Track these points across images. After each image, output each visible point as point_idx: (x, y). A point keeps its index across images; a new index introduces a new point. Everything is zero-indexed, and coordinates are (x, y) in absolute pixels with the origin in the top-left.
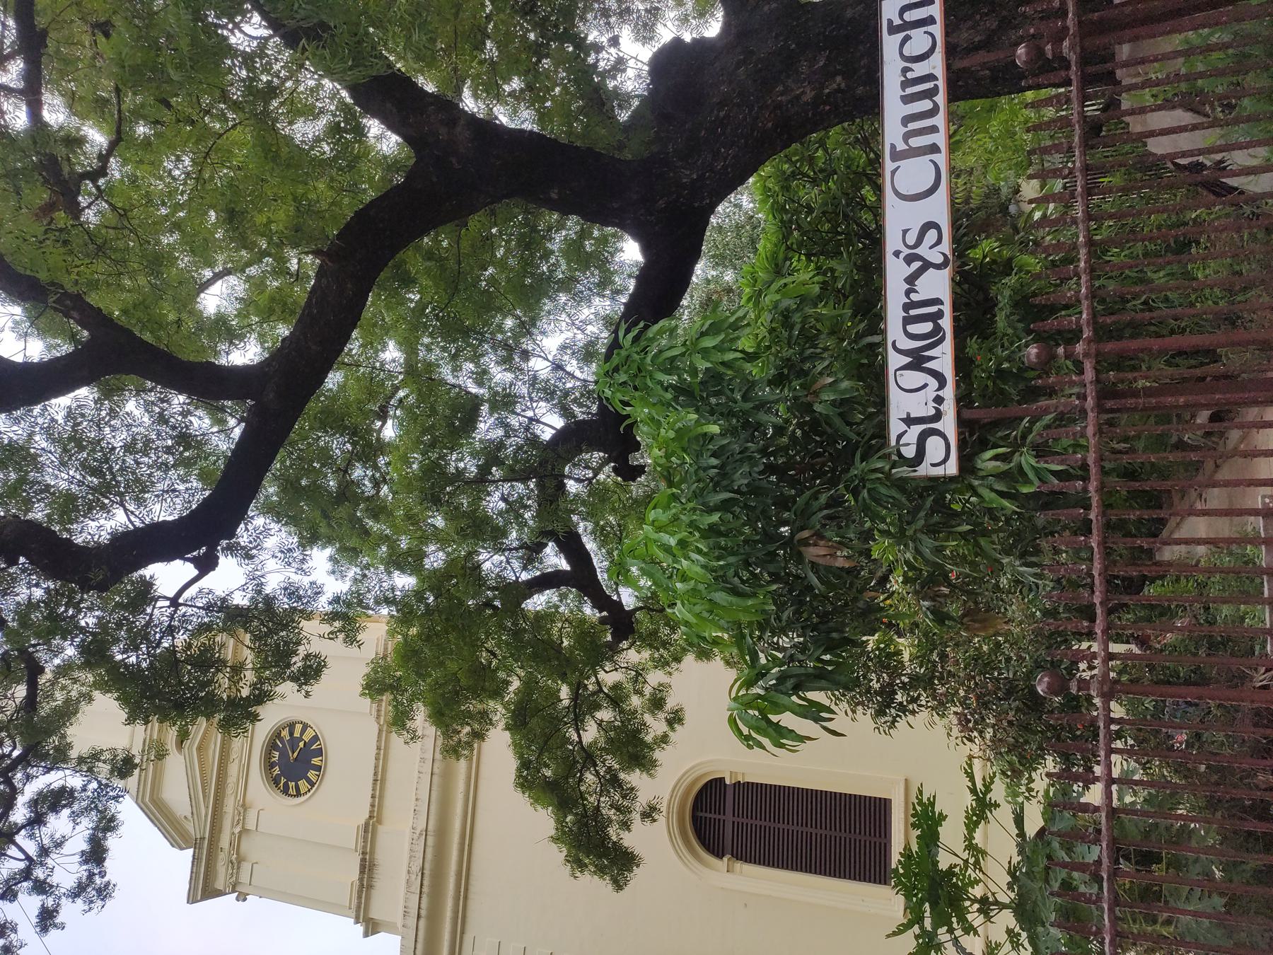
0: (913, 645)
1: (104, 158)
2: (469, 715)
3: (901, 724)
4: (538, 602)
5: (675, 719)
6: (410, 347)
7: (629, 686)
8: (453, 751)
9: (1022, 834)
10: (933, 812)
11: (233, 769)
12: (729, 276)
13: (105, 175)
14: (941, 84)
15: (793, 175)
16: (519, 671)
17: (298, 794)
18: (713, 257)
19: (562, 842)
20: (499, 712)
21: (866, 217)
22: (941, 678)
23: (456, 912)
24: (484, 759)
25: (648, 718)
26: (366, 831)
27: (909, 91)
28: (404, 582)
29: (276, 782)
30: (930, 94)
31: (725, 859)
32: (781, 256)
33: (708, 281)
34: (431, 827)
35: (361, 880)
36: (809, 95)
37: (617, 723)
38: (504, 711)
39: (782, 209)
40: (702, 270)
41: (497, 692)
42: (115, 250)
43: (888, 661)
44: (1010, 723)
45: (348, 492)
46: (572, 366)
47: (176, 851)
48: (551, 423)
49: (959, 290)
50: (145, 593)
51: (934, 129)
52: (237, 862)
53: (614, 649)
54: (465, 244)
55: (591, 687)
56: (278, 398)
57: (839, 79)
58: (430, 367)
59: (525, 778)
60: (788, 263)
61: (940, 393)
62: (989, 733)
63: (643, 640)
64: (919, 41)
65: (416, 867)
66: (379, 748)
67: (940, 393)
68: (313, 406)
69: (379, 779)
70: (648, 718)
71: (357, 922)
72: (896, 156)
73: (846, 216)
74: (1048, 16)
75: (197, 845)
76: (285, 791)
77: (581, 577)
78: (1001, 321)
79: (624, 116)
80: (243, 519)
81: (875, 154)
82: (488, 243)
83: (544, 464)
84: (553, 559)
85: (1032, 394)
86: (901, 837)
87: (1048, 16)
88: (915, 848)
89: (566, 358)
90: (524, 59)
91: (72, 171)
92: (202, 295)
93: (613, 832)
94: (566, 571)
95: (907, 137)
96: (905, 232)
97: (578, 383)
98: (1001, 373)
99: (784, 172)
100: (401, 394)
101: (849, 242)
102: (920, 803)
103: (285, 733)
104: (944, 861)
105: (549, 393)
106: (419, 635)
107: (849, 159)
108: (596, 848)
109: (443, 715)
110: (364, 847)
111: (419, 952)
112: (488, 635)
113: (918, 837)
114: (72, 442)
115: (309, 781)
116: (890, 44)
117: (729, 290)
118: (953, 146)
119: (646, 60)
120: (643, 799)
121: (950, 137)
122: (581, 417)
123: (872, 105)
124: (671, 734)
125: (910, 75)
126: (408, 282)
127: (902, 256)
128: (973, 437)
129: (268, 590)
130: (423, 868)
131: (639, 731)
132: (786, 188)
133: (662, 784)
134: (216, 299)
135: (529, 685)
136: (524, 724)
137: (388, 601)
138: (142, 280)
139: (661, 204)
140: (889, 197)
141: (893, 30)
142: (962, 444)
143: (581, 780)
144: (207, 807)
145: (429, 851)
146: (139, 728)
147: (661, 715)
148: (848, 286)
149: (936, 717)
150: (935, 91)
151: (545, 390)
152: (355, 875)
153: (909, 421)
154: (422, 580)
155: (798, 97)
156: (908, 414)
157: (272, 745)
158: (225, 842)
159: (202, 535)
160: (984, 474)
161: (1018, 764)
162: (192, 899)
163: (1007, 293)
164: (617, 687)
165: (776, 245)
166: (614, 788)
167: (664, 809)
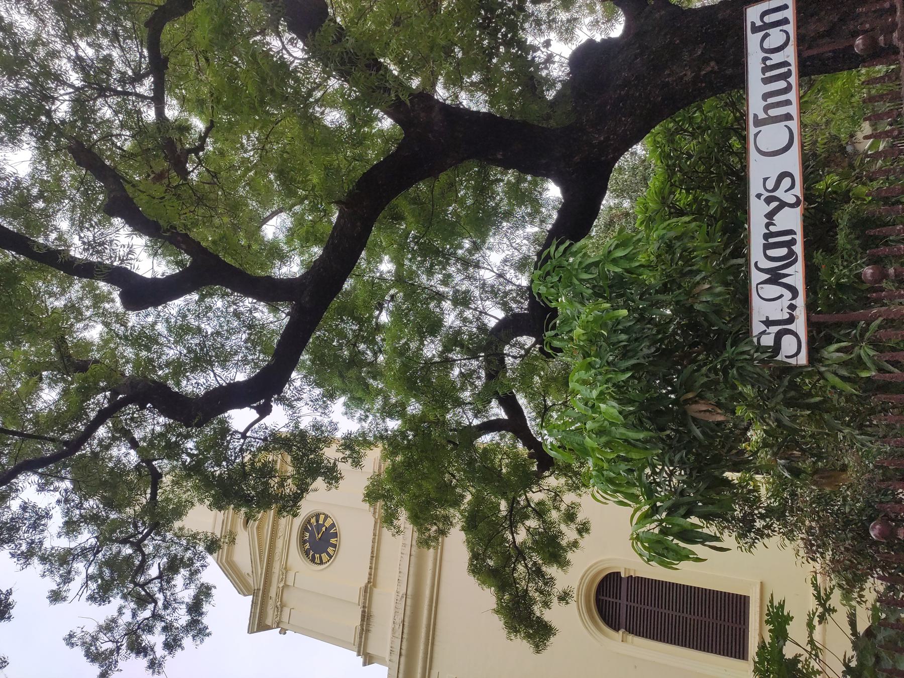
0: (769, 483)
1: (203, 139)
2: (437, 517)
3: (759, 544)
4: (486, 439)
5: (583, 529)
6: (398, 261)
7: (549, 503)
8: (425, 543)
9: (854, 633)
10: (783, 612)
11: (280, 543)
12: (626, 204)
13: (203, 149)
14: (793, 68)
15: (677, 131)
16: (471, 489)
17: (321, 563)
18: (614, 190)
19: (502, 614)
20: (457, 517)
21: (733, 160)
22: (791, 511)
23: (426, 653)
24: (445, 548)
25: (563, 527)
26: (366, 592)
27: (768, 74)
28: (393, 424)
29: (307, 553)
30: (785, 76)
31: (621, 632)
32: (666, 191)
33: (611, 208)
35: (362, 625)
36: (690, 75)
37: (540, 530)
38: (460, 517)
39: (668, 157)
40: (608, 201)
41: (456, 502)
42: (210, 200)
43: (751, 499)
44: (847, 549)
45: (356, 361)
46: (511, 274)
47: (241, 596)
48: (495, 315)
49: (807, 214)
50: (224, 430)
51: (788, 103)
52: (280, 608)
53: (539, 476)
54: (437, 191)
55: (522, 503)
56: (312, 299)
57: (713, 63)
58: (412, 273)
59: (475, 566)
60: (672, 196)
61: (793, 302)
62: (829, 555)
63: (561, 470)
64: (776, 37)
65: (399, 620)
66: (375, 535)
67: (793, 302)
68: (335, 303)
69: (375, 557)
70: (563, 527)
71: (359, 655)
72: (758, 123)
73: (717, 161)
74: (882, 13)
75: (255, 594)
76: (313, 560)
77: (515, 424)
78: (841, 239)
79: (550, 95)
80: (288, 381)
81: (740, 113)
82: (452, 187)
83: (490, 344)
84: (497, 411)
85: (866, 303)
86: (756, 632)
87: (882, 13)
88: (768, 640)
89: (506, 268)
90: (481, 60)
91: (182, 149)
92: (264, 227)
93: (537, 609)
94: (504, 420)
95: (766, 108)
96: (765, 180)
97: (514, 287)
98: (840, 286)
99: (669, 130)
100: (392, 292)
101: (720, 180)
102: (772, 606)
103: (313, 521)
104: (789, 651)
105: (492, 292)
106: (402, 463)
107: (719, 118)
108: (524, 619)
109: (419, 518)
110: (364, 603)
111: (401, 676)
112: (450, 462)
113: (770, 631)
114: (181, 331)
115: (328, 554)
116: (753, 41)
117: (627, 214)
118: (803, 107)
119: (567, 56)
120: (559, 587)
121: (801, 98)
122: (517, 311)
123: (739, 80)
124: (580, 541)
125: (768, 63)
126: (398, 217)
127: (763, 198)
128: (819, 336)
129: (302, 426)
130: (404, 621)
131: (556, 537)
132: (671, 141)
133: (574, 575)
134: (274, 229)
135: (478, 500)
136: (475, 527)
137: (382, 437)
138: (226, 219)
139: (577, 159)
140: (753, 154)
141: (755, 29)
142: (811, 340)
143: (514, 569)
144: (262, 568)
145: (408, 608)
146: (220, 515)
147: (573, 526)
148: (719, 212)
149: (787, 542)
150: (788, 74)
151: (492, 292)
152: (358, 622)
153: (768, 323)
154: (405, 422)
155: (681, 78)
156: (767, 317)
157: (304, 529)
158: (273, 593)
159: (263, 390)
160: (830, 362)
161: (852, 582)
162: (251, 631)
163: (846, 217)
164: (541, 503)
165: (663, 183)
166: (538, 577)
167: (575, 595)
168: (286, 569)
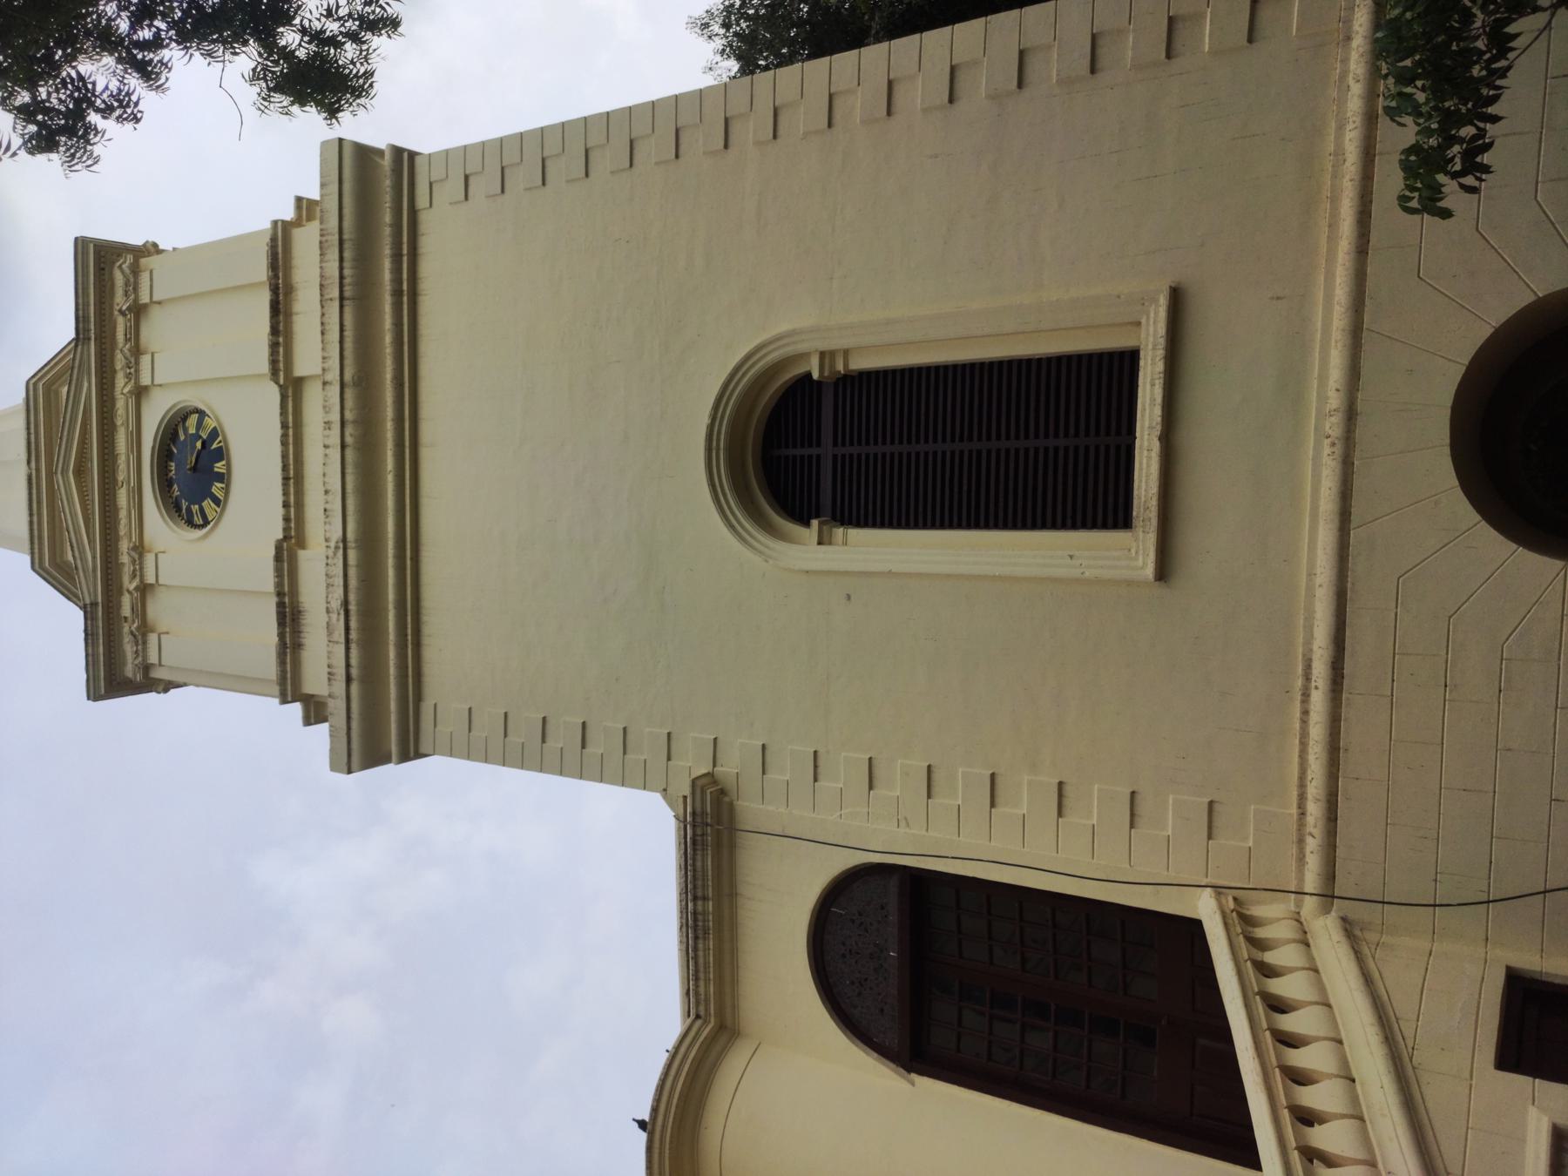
11: (122, 497)
17: (206, 522)
23: (402, 667)
31: (815, 523)
34: (351, 535)
35: (281, 636)
65: (336, 603)
66: (284, 426)
71: (284, 701)
76: (190, 523)
115: (217, 501)
144: (93, 550)
168: (140, 549)
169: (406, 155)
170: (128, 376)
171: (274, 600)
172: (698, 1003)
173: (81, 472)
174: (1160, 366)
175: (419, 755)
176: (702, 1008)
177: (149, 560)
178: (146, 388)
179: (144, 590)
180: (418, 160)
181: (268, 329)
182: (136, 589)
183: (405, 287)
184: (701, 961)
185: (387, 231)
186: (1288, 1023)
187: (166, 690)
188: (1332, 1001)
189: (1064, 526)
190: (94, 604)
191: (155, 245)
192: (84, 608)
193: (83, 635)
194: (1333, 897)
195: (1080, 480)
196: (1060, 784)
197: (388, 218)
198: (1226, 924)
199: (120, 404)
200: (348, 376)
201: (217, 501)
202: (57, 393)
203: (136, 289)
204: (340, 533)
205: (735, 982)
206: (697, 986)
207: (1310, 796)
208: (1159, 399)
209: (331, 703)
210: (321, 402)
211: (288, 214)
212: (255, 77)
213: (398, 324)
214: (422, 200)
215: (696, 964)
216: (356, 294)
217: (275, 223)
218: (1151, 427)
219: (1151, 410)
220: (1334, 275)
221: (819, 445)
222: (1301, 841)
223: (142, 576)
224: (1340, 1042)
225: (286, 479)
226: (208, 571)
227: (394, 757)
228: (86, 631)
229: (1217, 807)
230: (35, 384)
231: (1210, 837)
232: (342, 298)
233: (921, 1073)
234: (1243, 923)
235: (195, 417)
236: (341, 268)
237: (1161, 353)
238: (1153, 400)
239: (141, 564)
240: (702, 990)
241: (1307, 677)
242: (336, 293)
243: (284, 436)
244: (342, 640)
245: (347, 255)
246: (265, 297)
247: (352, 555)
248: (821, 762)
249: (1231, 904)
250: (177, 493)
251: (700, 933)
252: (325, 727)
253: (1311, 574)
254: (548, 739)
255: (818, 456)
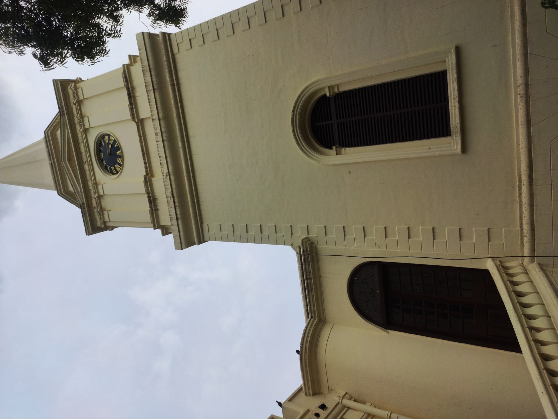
11: (86, 167)
17: (117, 172)
31: (334, 148)
35: (151, 207)
65: (169, 194)
66: (140, 136)
71: (155, 229)
76: (112, 173)
115: (120, 165)
144: (79, 186)
168: (96, 184)
169: (167, 35)
170: (81, 125)
171: (146, 196)
172: (311, 313)
173: (70, 160)
174: (455, 76)
175: (204, 241)
176: (313, 314)
177: (100, 187)
178: (88, 129)
179: (100, 197)
180: (171, 36)
181: (128, 103)
182: (97, 197)
183: (175, 82)
184: (311, 299)
185: (165, 63)
186: (525, 300)
187: (112, 230)
188: (539, 292)
189: (421, 138)
190: (83, 204)
191: (80, 79)
192: (81, 206)
193: (81, 214)
194: (535, 257)
195: (386, 121)
196: (433, 228)
197: (165, 58)
198: (498, 270)
199: (79, 135)
200: (161, 116)
201: (120, 165)
202: (56, 135)
203: (77, 95)
204: (167, 170)
205: (323, 305)
206: (310, 307)
207: (524, 223)
208: (456, 88)
209: (172, 227)
210: (153, 127)
211: (127, 61)
212: (150, 15)
213: (175, 96)
214: (175, 51)
215: (310, 300)
216: (158, 87)
217: (124, 65)
218: (454, 98)
219: (454, 93)
220: (515, 35)
221: (331, 120)
222: (522, 239)
223: (98, 193)
224: (544, 305)
225: (143, 154)
226: (121, 188)
227: (196, 243)
228: (82, 213)
229: (491, 230)
230: (47, 132)
231: (489, 241)
232: (154, 89)
233: (391, 329)
234: (504, 269)
235: (107, 137)
236: (152, 79)
237: (455, 71)
238: (454, 88)
239: (97, 189)
240: (312, 308)
241: (520, 181)
242: (151, 88)
243: (140, 140)
244: (173, 206)
245: (153, 73)
246: (125, 92)
247: (172, 177)
248: (346, 230)
249: (499, 263)
250: (105, 164)
251: (310, 290)
252: (171, 235)
253: (518, 145)
254: (249, 231)
255: (332, 124)
